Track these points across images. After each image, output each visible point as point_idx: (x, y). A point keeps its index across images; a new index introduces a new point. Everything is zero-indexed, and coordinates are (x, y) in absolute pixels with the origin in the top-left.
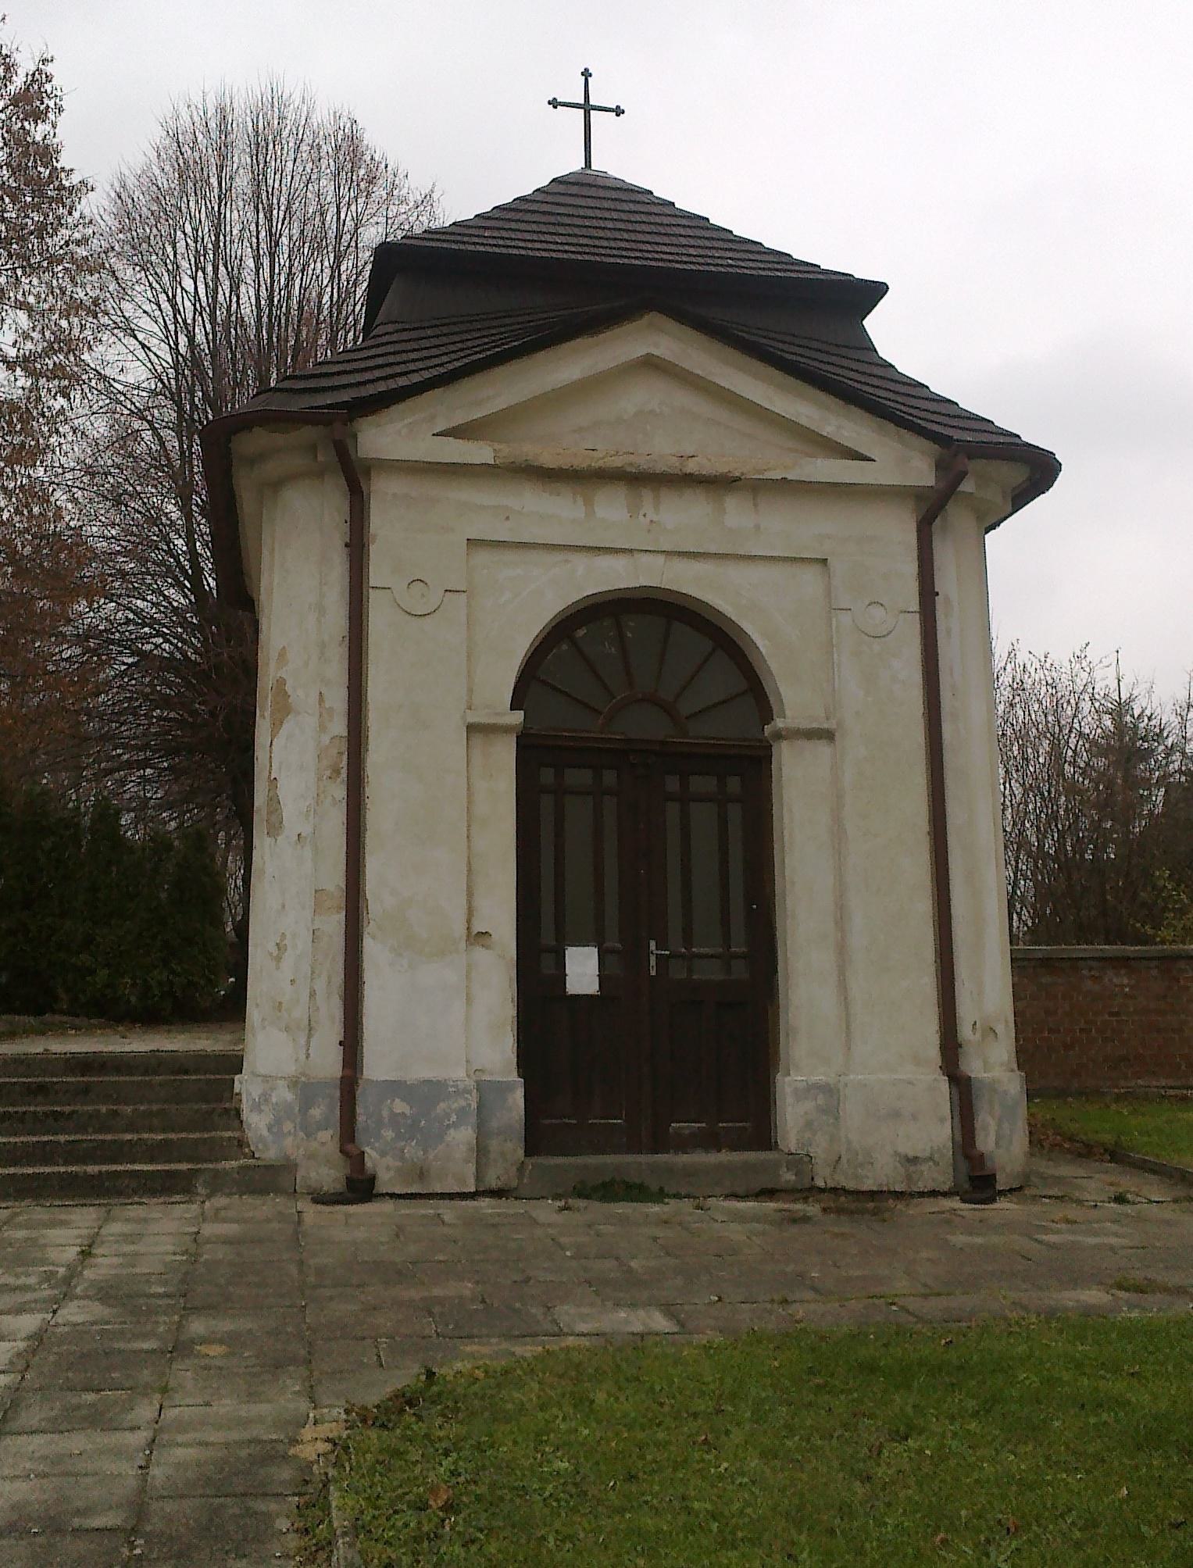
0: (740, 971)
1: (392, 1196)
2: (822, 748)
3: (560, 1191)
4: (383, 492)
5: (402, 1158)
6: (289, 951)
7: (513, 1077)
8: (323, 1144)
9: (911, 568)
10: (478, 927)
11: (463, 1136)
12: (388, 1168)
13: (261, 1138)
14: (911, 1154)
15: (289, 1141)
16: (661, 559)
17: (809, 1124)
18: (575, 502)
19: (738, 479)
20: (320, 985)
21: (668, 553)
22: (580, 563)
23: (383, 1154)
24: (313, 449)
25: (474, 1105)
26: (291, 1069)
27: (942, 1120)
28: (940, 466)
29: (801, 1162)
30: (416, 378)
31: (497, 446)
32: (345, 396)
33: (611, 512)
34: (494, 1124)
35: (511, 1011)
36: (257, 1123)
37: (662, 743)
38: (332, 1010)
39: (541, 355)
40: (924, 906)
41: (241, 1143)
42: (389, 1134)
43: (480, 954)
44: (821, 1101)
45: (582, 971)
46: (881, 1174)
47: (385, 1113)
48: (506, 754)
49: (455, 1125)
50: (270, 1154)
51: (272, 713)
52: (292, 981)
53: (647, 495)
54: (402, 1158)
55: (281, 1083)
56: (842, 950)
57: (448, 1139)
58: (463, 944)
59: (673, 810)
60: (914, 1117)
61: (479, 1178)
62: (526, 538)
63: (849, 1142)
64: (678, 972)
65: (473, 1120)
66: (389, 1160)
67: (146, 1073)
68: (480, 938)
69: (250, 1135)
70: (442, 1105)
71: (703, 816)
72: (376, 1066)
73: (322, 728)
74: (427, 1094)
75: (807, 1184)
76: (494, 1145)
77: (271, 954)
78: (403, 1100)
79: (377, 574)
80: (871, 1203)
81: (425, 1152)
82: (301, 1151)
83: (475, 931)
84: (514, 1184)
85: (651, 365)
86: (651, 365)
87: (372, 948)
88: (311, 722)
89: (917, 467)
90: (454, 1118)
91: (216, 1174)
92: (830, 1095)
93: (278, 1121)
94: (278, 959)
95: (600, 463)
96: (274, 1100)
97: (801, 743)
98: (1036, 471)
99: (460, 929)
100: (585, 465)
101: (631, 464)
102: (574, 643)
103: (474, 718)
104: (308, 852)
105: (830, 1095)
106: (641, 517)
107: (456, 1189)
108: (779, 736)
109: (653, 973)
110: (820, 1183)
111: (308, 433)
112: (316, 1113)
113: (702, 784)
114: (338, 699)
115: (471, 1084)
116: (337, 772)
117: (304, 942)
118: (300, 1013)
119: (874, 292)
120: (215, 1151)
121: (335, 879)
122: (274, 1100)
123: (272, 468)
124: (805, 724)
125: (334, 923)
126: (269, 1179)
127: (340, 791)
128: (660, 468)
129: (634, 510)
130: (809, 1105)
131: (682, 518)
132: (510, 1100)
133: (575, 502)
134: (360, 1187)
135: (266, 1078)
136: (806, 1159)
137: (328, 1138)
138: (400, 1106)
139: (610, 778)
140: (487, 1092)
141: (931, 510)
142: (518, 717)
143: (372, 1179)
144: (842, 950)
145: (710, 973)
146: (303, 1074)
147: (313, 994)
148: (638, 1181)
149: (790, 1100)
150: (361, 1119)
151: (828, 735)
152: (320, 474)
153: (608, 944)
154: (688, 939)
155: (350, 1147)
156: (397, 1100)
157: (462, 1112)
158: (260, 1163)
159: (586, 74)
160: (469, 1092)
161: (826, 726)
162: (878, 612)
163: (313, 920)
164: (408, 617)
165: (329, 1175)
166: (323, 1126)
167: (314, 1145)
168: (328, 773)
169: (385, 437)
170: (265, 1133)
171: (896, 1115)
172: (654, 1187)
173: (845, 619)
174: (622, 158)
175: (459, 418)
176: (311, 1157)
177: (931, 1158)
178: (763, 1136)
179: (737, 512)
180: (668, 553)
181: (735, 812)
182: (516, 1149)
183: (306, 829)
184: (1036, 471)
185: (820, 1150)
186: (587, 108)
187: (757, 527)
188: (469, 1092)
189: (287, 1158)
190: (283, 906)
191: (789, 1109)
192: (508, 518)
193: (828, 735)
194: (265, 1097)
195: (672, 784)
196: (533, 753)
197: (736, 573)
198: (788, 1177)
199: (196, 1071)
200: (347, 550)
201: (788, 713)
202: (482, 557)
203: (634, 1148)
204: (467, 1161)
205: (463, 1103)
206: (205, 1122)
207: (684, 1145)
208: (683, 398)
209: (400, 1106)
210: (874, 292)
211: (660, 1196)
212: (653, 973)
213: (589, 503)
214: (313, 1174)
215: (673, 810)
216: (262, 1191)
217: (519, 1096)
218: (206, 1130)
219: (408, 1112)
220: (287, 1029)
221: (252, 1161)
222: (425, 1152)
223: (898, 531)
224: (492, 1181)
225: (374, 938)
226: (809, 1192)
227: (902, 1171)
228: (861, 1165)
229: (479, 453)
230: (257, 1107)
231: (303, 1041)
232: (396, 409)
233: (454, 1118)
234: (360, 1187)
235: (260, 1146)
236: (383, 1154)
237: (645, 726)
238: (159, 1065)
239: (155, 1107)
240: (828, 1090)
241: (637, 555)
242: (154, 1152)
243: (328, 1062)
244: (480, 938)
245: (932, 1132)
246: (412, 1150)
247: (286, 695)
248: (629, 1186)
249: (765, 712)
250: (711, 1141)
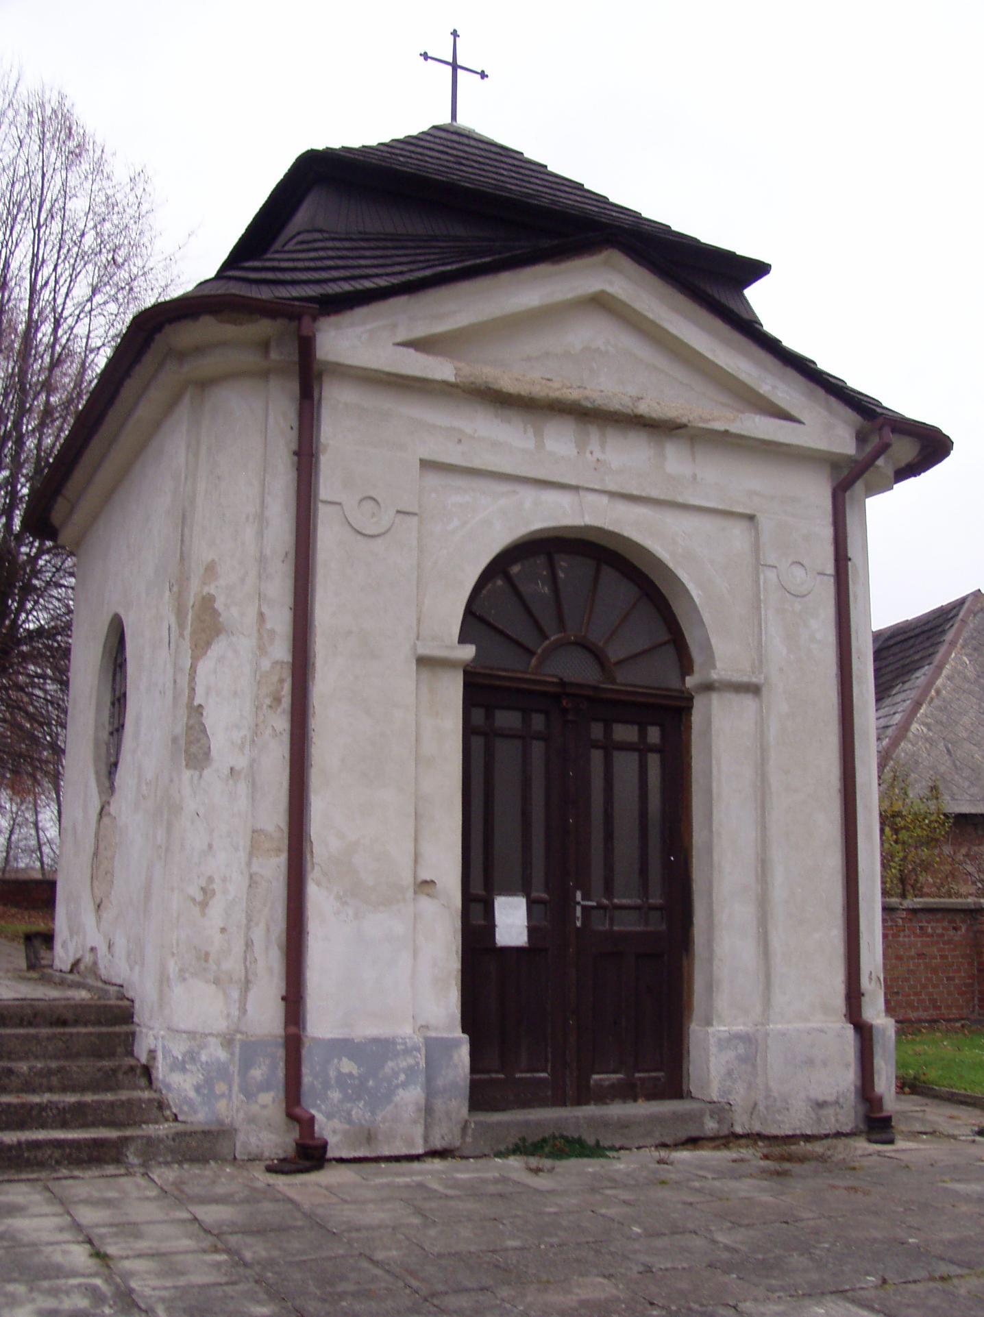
0: (657, 925)
1: (341, 1160)
2: (748, 702)
3: (502, 1148)
4: (336, 400)
5: (349, 1121)
6: (218, 896)
7: (458, 1033)
8: (264, 1107)
9: (828, 532)
10: (425, 875)
11: (411, 1096)
12: (334, 1132)
13: (188, 1101)
14: (821, 1098)
15: (221, 1105)
16: (605, 499)
17: (730, 1073)
18: (525, 432)
19: (682, 426)
20: (258, 934)
21: (613, 495)
22: (528, 495)
23: (330, 1116)
24: (265, 346)
25: (423, 1064)
26: (221, 1025)
27: (847, 1066)
28: (861, 438)
29: (721, 1110)
30: (382, 282)
31: (461, 365)
32: (311, 291)
33: (559, 446)
34: (440, 1083)
35: (455, 964)
36: (178, 1083)
37: (595, 688)
38: (270, 964)
39: (505, 276)
40: (834, 861)
41: (161, 1105)
42: (335, 1095)
43: (427, 905)
44: (741, 1050)
45: (512, 921)
46: (795, 1120)
47: (332, 1074)
48: (452, 690)
49: (404, 1085)
50: (200, 1118)
51: (193, 633)
52: (223, 930)
53: (594, 434)
54: (349, 1121)
55: (212, 1040)
56: (763, 903)
57: (397, 1099)
58: (410, 893)
59: (597, 756)
60: (825, 1064)
61: (426, 1140)
62: (477, 463)
63: (768, 1089)
64: (601, 925)
65: (422, 1079)
66: (336, 1124)
67: (21, 1024)
68: (425, 886)
69: (171, 1098)
70: (390, 1064)
71: (626, 764)
72: (320, 1024)
73: (262, 649)
74: (376, 1052)
75: (725, 1131)
76: (439, 1104)
77: (194, 900)
78: (350, 1059)
79: (327, 487)
80: (783, 1150)
81: (373, 1113)
82: (241, 1115)
83: (419, 880)
84: (458, 1143)
85: (601, 303)
86: (601, 303)
87: (317, 895)
88: (247, 643)
89: (834, 434)
90: (402, 1077)
91: (150, 1142)
92: (750, 1047)
93: (209, 1082)
94: (204, 905)
95: (557, 394)
96: (204, 1058)
97: (730, 696)
98: (930, 446)
99: (407, 879)
100: (543, 394)
101: (587, 398)
102: (508, 579)
103: (423, 651)
104: (242, 788)
105: (750, 1047)
106: (588, 455)
107: (404, 1151)
108: (709, 687)
109: (579, 924)
110: (738, 1130)
111: (264, 327)
112: (257, 1073)
113: (625, 733)
114: (281, 621)
115: (418, 1040)
116: (277, 700)
117: (236, 887)
118: (232, 964)
119: (758, 270)
120: (131, 1114)
121: (275, 818)
122: (204, 1058)
123: (208, 365)
124: (737, 678)
125: (274, 867)
126: (204, 1146)
127: (282, 723)
128: (615, 405)
129: (581, 446)
130: (730, 1054)
131: (626, 458)
132: (456, 1057)
133: (525, 432)
134: (310, 1155)
135: (192, 1034)
136: (727, 1107)
137: (270, 1102)
138: (348, 1066)
139: (538, 722)
140: (436, 1049)
141: (851, 480)
142: (468, 652)
143: (324, 1146)
144: (763, 903)
145: (628, 924)
146: (238, 1031)
147: (249, 944)
148: (576, 1136)
149: (713, 1050)
150: (307, 1079)
151: (753, 689)
152: (264, 375)
153: (534, 895)
154: (609, 891)
155: (297, 1111)
156: (345, 1060)
157: (411, 1071)
158: (189, 1128)
159: (455, 34)
160: (418, 1050)
161: (754, 680)
162: (799, 572)
163: (249, 864)
164: (359, 537)
165: (274, 1139)
166: (266, 1086)
167: (255, 1108)
168: (268, 701)
169: (347, 341)
170: (192, 1094)
171: (810, 1062)
172: (591, 1141)
173: (771, 575)
174: (495, 118)
175: (421, 330)
176: (252, 1120)
177: (837, 1102)
178: (673, 1084)
179: (676, 461)
180: (613, 495)
181: (654, 760)
182: (459, 1106)
183: (241, 762)
184: (930, 446)
185: (739, 1096)
186: (455, 66)
187: (694, 477)
188: (418, 1050)
189: (221, 1123)
190: (210, 846)
191: (712, 1059)
192: (460, 441)
193: (753, 689)
194: (192, 1056)
195: (597, 730)
196: (480, 691)
197: (674, 523)
198: (711, 1126)
199: (76, 1023)
200: (296, 458)
201: (718, 665)
202: (434, 480)
203: (560, 1101)
204: (415, 1122)
205: (411, 1061)
206: (108, 1081)
207: (603, 1096)
208: (627, 341)
209: (348, 1066)
210: (758, 270)
211: (596, 1151)
212: (579, 924)
213: (539, 434)
214: (253, 1140)
215: (597, 756)
216: (201, 1159)
217: (463, 1054)
218: (110, 1089)
219: (355, 1072)
220: (217, 982)
221: (180, 1127)
222: (373, 1113)
223: (816, 493)
224: (438, 1144)
225: (318, 884)
226: (728, 1139)
227: (813, 1116)
228: (779, 1111)
229: (441, 369)
230: (179, 1066)
231: (235, 994)
232: (361, 312)
233: (402, 1077)
234: (310, 1155)
235: (185, 1108)
236: (330, 1116)
237: (575, 669)
238: (35, 1015)
239: (54, 1065)
240: (746, 1039)
241: (582, 493)
242: (65, 1117)
243: (266, 1016)
244: (425, 886)
245: (847, 1078)
246: (359, 1112)
247: (215, 614)
248: (570, 1141)
249: (685, 664)
250: (628, 1092)
